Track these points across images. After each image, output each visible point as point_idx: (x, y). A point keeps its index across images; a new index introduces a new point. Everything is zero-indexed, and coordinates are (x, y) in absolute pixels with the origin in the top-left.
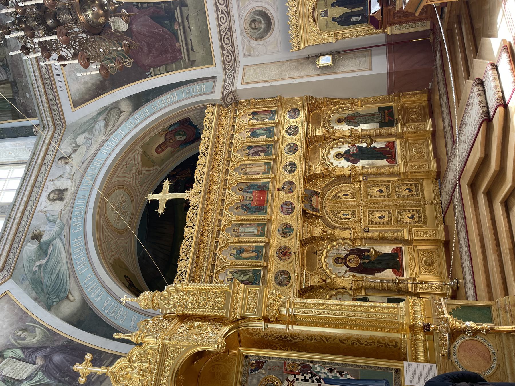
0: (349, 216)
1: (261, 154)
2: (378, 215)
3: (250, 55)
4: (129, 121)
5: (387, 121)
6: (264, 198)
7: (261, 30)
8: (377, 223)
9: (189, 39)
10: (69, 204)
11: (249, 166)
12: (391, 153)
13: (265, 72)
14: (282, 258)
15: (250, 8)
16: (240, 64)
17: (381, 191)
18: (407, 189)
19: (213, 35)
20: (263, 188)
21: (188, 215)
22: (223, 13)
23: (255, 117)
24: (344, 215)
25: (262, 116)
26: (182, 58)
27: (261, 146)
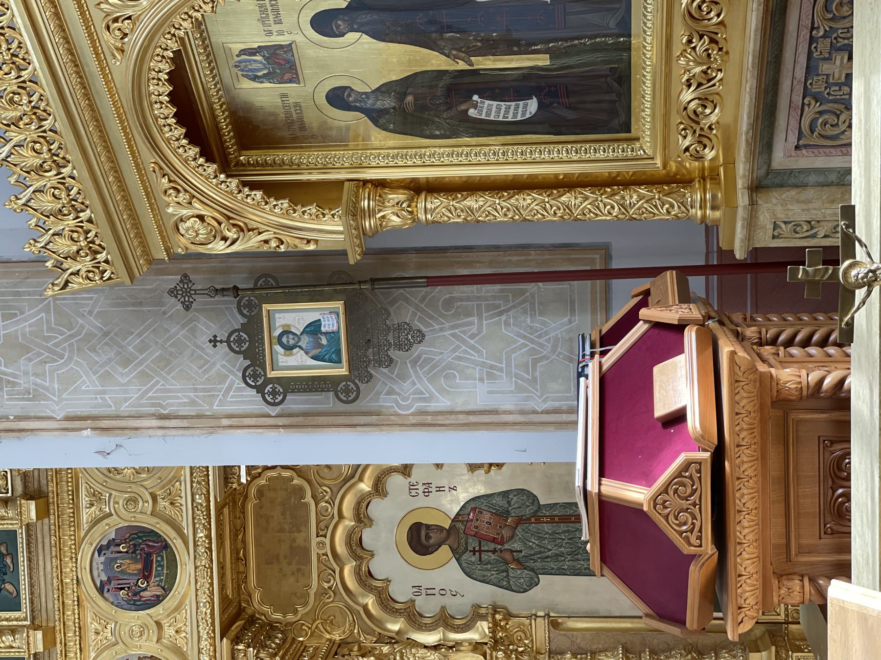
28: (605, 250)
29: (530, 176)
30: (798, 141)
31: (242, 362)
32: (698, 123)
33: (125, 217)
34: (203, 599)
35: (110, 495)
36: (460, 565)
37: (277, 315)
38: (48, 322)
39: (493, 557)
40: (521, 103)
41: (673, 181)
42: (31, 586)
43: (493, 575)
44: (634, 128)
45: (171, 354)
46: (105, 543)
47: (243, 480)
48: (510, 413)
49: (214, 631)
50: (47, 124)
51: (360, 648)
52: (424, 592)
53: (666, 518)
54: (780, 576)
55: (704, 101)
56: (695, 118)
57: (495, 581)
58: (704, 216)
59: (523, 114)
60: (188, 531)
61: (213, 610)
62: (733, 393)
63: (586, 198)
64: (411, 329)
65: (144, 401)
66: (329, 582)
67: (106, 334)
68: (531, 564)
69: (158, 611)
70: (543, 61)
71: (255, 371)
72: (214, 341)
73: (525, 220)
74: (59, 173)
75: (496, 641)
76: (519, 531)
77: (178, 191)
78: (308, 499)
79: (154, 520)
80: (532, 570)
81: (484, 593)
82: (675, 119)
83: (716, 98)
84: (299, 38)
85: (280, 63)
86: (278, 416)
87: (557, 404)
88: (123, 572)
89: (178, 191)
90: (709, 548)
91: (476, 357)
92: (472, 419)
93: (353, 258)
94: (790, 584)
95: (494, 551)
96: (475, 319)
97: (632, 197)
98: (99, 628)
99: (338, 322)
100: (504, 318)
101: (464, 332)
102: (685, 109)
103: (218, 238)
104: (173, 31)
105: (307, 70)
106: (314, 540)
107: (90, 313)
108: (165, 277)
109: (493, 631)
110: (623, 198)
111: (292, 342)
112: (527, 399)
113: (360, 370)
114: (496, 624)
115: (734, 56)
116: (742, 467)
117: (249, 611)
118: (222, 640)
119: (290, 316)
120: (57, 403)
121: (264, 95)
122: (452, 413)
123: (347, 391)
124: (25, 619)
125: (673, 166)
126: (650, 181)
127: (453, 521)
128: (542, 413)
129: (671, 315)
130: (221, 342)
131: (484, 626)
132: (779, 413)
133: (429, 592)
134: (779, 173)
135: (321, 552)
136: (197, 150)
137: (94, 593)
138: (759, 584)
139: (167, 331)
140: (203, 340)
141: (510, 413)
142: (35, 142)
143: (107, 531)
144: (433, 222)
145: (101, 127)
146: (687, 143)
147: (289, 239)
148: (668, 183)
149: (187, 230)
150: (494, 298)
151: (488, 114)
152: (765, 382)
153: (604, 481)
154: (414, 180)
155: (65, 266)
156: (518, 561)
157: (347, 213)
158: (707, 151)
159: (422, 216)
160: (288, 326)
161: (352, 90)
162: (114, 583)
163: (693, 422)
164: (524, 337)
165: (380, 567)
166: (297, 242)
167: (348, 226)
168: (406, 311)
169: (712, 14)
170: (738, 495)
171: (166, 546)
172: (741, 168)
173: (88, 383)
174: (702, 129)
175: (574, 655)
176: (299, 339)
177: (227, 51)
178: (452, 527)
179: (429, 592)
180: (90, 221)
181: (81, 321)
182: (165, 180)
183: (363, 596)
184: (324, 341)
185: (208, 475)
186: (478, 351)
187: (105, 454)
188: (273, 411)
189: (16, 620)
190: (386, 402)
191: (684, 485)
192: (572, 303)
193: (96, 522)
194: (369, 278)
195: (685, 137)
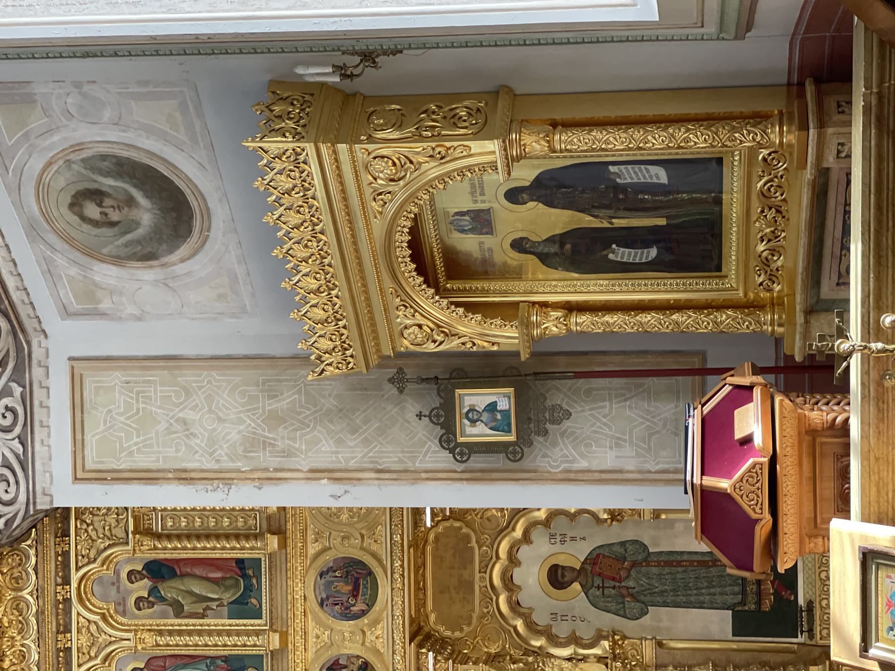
5: (767, 606)
13: (189, 415)
15: (58, 141)
16: (50, 343)
23: (168, 590)
25: (198, 588)
28: (703, 355)
29: (650, 301)
30: (839, 279)
31: (439, 431)
32: (769, 266)
33: (366, 324)
34: (398, 613)
35: (330, 534)
36: (588, 597)
37: (466, 398)
38: (300, 401)
39: (613, 592)
40: (646, 251)
42: (271, 600)
43: (613, 606)
44: (724, 269)
45: (386, 425)
46: (325, 569)
47: (429, 524)
48: (632, 472)
49: (404, 638)
50: (326, 261)
51: (511, 658)
52: (559, 618)
53: (742, 496)
54: (810, 537)
55: (773, 251)
56: (767, 263)
57: (614, 610)
58: (773, 330)
59: (647, 257)
61: (404, 622)
62: (781, 425)
63: (690, 317)
64: (562, 408)
65: (365, 459)
66: (487, 608)
67: (341, 410)
68: (642, 598)
70: (662, 222)
71: (448, 438)
72: (420, 416)
73: (646, 331)
74: (329, 294)
75: (615, 656)
76: (633, 572)
77: (406, 307)
78: (474, 543)
79: (362, 553)
80: (643, 602)
81: (608, 620)
82: (753, 263)
83: (782, 250)
84: (495, 205)
85: (481, 221)
86: (462, 472)
87: (666, 466)
88: (338, 592)
89: (406, 307)
90: (768, 517)
91: (607, 431)
92: (604, 476)
93: (524, 356)
94: (816, 540)
95: (614, 588)
96: (607, 403)
97: (723, 317)
98: (319, 633)
99: (510, 404)
100: (628, 403)
101: (599, 413)
102: (760, 256)
103: (430, 341)
104: (416, 201)
106: (477, 576)
107: (330, 395)
108: (384, 370)
109: (613, 648)
110: (716, 317)
111: (475, 417)
112: (645, 462)
114: (615, 642)
115: (793, 219)
117: (426, 629)
118: (410, 644)
119: (475, 398)
120: (304, 460)
121: (469, 244)
122: (589, 471)
123: (514, 453)
124: (266, 625)
125: (751, 295)
126: (735, 306)
127: (583, 563)
128: (655, 472)
129: (746, 381)
130: (425, 416)
131: (606, 644)
132: (811, 438)
133: (564, 618)
134: (826, 301)
135: (482, 585)
136: (422, 279)
137: (317, 608)
138: (797, 540)
139: (384, 409)
140: (411, 415)
141: (632, 472)
142: (317, 273)
144: (582, 332)
145: (360, 264)
146: (761, 280)
147: (480, 342)
148: (748, 308)
149: (410, 334)
150: (622, 388)
151: (622, 257)
152: (801, 419)
153: (704, 477)
154: (568, 302)
155: (323, 359)
156: (632, 595)
157: (522, 324)
158: (775, 285)
159: (573, 328)
160: (474, 405)
161: (529, 240)
162: (331, 600)
163: (758, 441)
164: (642, 417)
165: (523, 597)
166: (485, 344)
167: (522, 334)
168: (558, 394)
169: (778, 194)
170: (784, 485)
171: (370, 573)
172: (799, 298)
174: (771, 270)
175: (675, 668)
176: (481, 416)
177: (446, 214)
178: (582, 568)
179: (564, 618)
180: (344, 327)
181: (322, 401)
182: (398, 300)
183: (513, 619)
184: (499, 417)
185: (402, 520)
186: (609, 427)
187: (336, 497)
188: (462, 466)
189: (259, 625)
190: (541, 463)
191: (752, 477)
192: (678, 393)
194: (532, 372)
195: (760, 276)
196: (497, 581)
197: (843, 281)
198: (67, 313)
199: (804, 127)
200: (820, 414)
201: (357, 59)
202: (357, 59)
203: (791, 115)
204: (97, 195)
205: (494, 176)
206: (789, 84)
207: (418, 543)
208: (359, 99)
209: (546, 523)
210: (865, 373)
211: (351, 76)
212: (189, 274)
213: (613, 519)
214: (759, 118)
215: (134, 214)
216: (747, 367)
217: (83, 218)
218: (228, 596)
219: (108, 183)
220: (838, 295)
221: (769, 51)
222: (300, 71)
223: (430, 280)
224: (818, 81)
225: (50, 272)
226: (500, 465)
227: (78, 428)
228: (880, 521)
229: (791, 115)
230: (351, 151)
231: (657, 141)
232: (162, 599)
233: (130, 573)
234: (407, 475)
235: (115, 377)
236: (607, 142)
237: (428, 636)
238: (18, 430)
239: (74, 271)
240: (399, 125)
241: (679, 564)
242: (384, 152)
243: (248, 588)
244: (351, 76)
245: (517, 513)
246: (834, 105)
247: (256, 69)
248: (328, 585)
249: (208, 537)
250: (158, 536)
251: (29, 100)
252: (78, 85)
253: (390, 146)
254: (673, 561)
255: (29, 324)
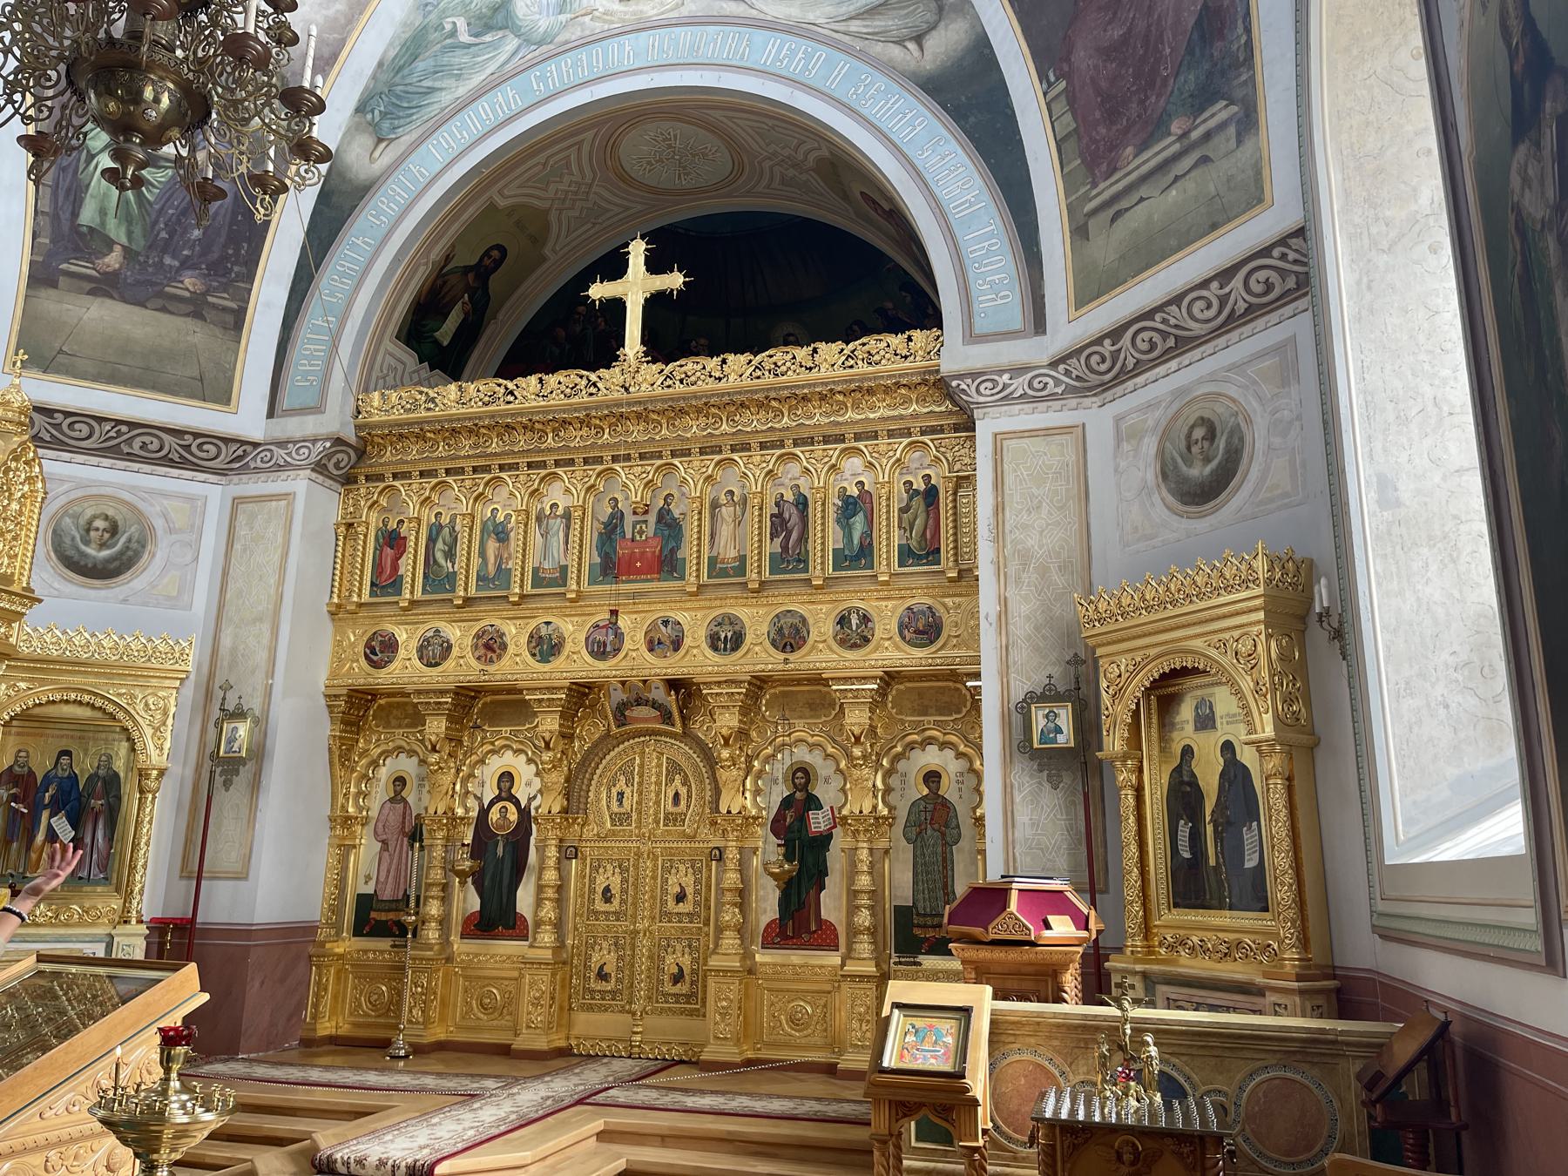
0: (615, 807)
1: (778, 541)
2: (616, 882)
3: (1119, 440)
4: (882, 82)
5: (917, 931)
6: (639, 572)
7: (1184, 468)
8: (593, 881)
9: (1143, 191)
10: (612, 22)
11: (739, 512)
12: (797, 935)
14: (481, 642)
15: (1252, 405)
16: (1095, 410)
17: (681, 898)
18: (681, 970)
19: (1148, 283)
20: (667, 564)
21: (573, 373)
22: (1223, 301)
23: (918, 502)
24: (621, 794)
26: (1094, 185)
27: (803, 538)
28: (1105, 891)
31: (1039, 691)
41: (1147, 930)
43: (913, 818)
55: (1193, 949)
56: (1183, 943)
60: (941, 654)
69: (898, 638)
70: (1212, 862)
72: (1050, 677)
81: (902, 814)
82: (1182, 932)
84: (1219, 733)
85: (1206, 721)
97: (1137, 907)
105: (1202, 735)
106: (932, 719)
113: (1035, 755)
114: (887, 819)
115: (1219, 966)
116: (1026, 954)
119: (1065, 718)
129: (1092, 925)
131: (885, 812)
143: (941, 612)
152: (1065, 967)
163: (1047, 933)
165: (916, 753)
172: (1156, 967)
173: (1025, 609)
190: (1017, 767)
193: (944, 605)
196: (928, 733)
197: (1171, 1004)
198: (1118, 420)
199: (1299, 978)
200: (1070, 981)
201: (1336, 625)
202: (1336, 625)
203: (1308, 968)
204: (1211, 435)
205: (1244, 732)
206: (1334, 968)
207: (954, 676)
208: (1301, 627)
209: (972, 770)
210: (1106, 1018)
211: (1321, 621)
212: (1153, 505)
213: (977, 819)
214: (1304, 942)
215: (1198, 463)
216: (1102, 926)
217: (1192, 427)
218: (913, 544)
219: (1221, 443)
220: (1159, 1001)
221: (1362, 951)
222: (1323, 581)
223: (1156, 684)
224: (1338, 991)
225: (1150, 406)
226: (1015, 736)
227: (1032, 433)
228: (992, 1022)
229: (1308, 968)
230: (1259, 622)
231: (1280, 861)
232: (911, 499)
233: (929, 476)
234: (1005, 672)
235: (1071, 457)
236: (1277, 821)
237: (888, 684)
238: (1030, 392)
239: (1151, 423)
240: (1282, 658)
241: (945, 868)
242: (1260, 648)
243: (920, 557)
244: (1321, 621)
245: (979, 748)
246: (1319, 1002)
247: (1323, 551)
248: (923, 613)
249: (955, 527)
250: (955, 494)
251: (1285, 383)
252: (1299, 418)
253: (1267, 650)
254: (947, 863)
255: (1109, 395)
